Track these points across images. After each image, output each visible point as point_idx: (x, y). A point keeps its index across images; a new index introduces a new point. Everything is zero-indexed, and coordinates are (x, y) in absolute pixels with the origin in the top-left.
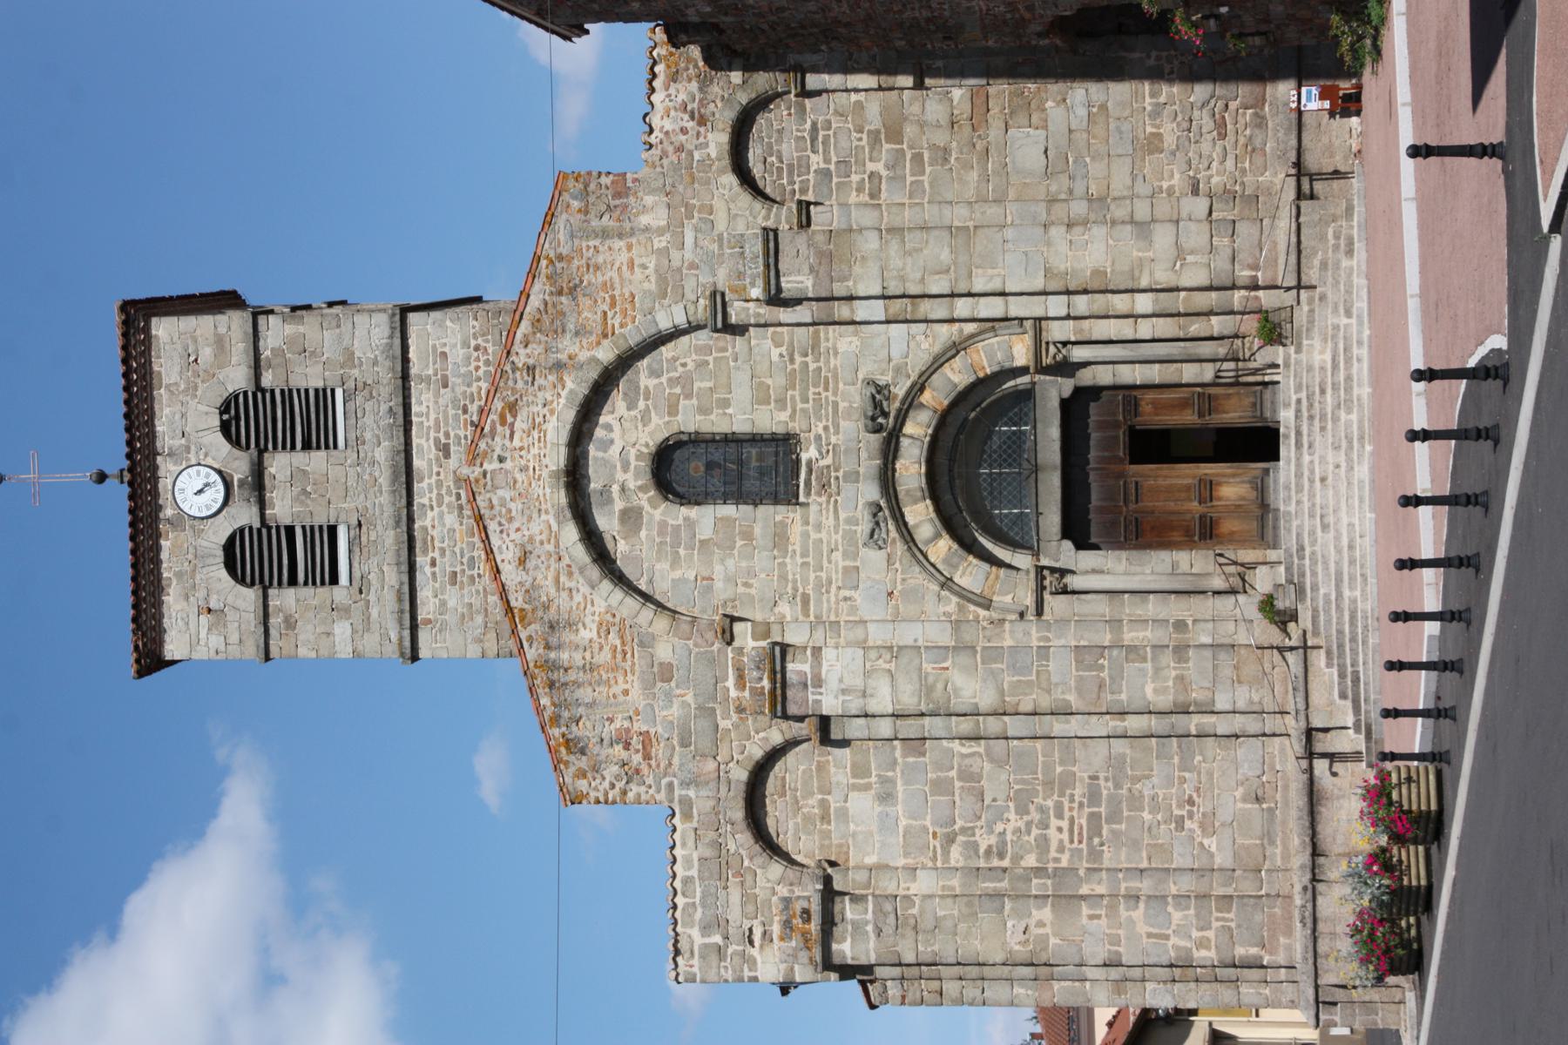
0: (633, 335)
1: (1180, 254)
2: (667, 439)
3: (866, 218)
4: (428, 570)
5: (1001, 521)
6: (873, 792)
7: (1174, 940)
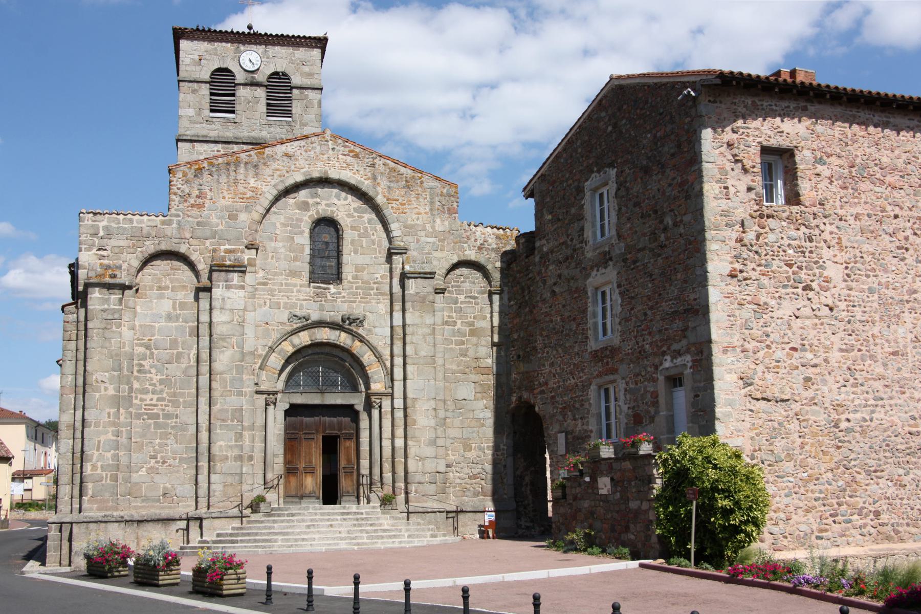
0: (388, 212)
1: (422, 459)
2: (340, 225)
3: (439, 320)
4: (216, 149)
7: (96, 453)
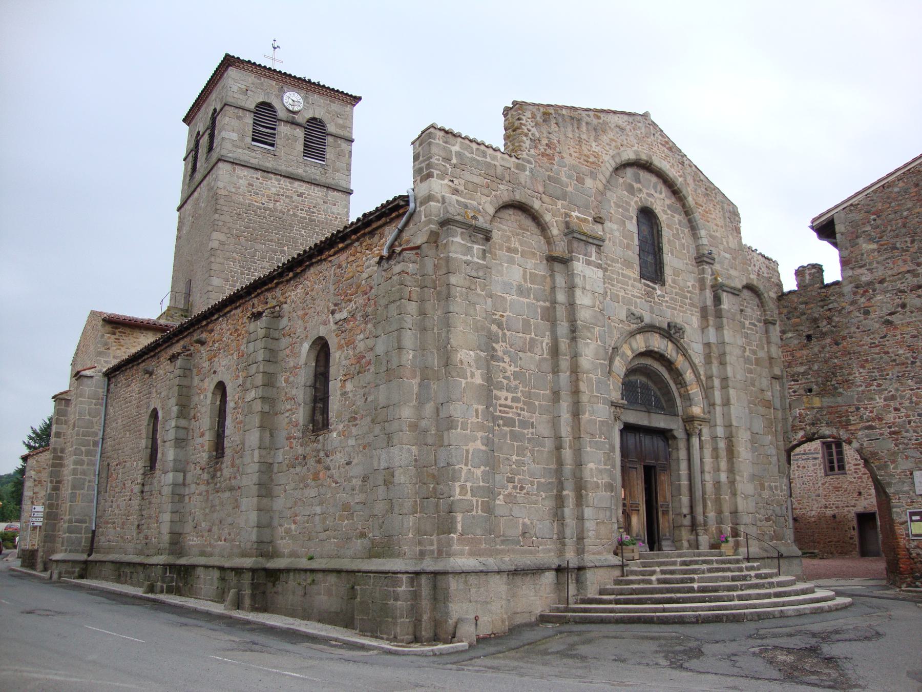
4: (255, 176)
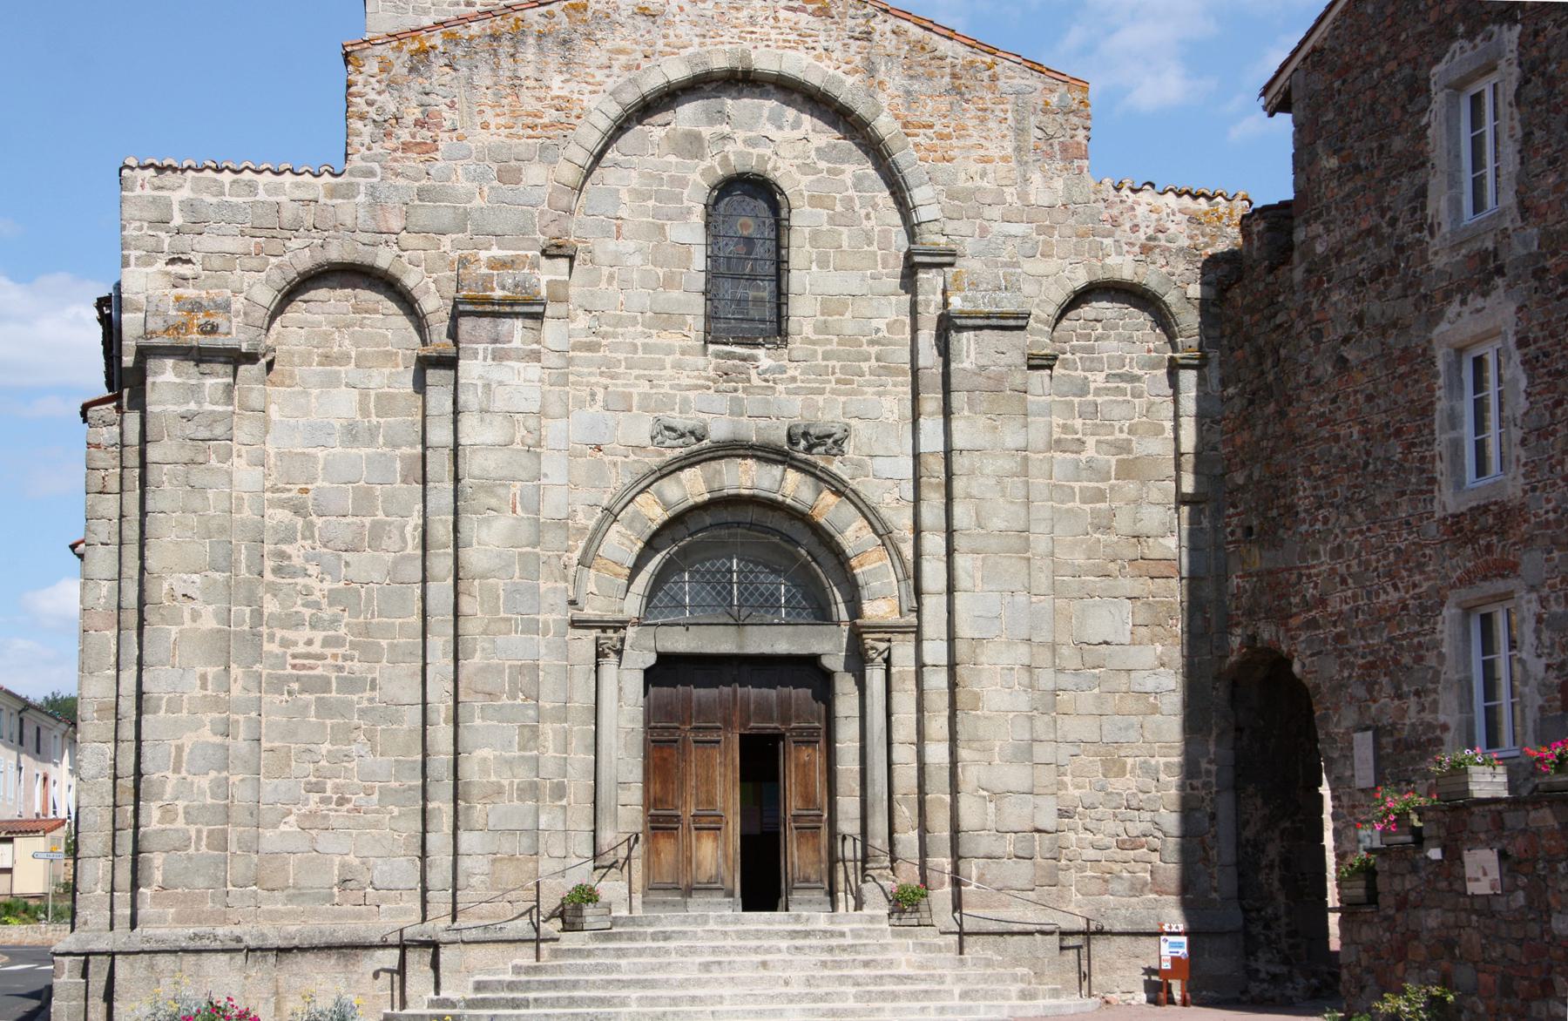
0: (906, 158)
1: (996, 796)
2: (782, 193)
3: (1037, 435)
5: (676, 583)
6: (358, 418)
7: (173, 778)
